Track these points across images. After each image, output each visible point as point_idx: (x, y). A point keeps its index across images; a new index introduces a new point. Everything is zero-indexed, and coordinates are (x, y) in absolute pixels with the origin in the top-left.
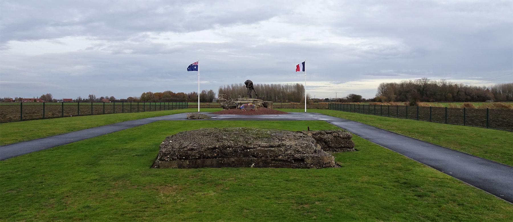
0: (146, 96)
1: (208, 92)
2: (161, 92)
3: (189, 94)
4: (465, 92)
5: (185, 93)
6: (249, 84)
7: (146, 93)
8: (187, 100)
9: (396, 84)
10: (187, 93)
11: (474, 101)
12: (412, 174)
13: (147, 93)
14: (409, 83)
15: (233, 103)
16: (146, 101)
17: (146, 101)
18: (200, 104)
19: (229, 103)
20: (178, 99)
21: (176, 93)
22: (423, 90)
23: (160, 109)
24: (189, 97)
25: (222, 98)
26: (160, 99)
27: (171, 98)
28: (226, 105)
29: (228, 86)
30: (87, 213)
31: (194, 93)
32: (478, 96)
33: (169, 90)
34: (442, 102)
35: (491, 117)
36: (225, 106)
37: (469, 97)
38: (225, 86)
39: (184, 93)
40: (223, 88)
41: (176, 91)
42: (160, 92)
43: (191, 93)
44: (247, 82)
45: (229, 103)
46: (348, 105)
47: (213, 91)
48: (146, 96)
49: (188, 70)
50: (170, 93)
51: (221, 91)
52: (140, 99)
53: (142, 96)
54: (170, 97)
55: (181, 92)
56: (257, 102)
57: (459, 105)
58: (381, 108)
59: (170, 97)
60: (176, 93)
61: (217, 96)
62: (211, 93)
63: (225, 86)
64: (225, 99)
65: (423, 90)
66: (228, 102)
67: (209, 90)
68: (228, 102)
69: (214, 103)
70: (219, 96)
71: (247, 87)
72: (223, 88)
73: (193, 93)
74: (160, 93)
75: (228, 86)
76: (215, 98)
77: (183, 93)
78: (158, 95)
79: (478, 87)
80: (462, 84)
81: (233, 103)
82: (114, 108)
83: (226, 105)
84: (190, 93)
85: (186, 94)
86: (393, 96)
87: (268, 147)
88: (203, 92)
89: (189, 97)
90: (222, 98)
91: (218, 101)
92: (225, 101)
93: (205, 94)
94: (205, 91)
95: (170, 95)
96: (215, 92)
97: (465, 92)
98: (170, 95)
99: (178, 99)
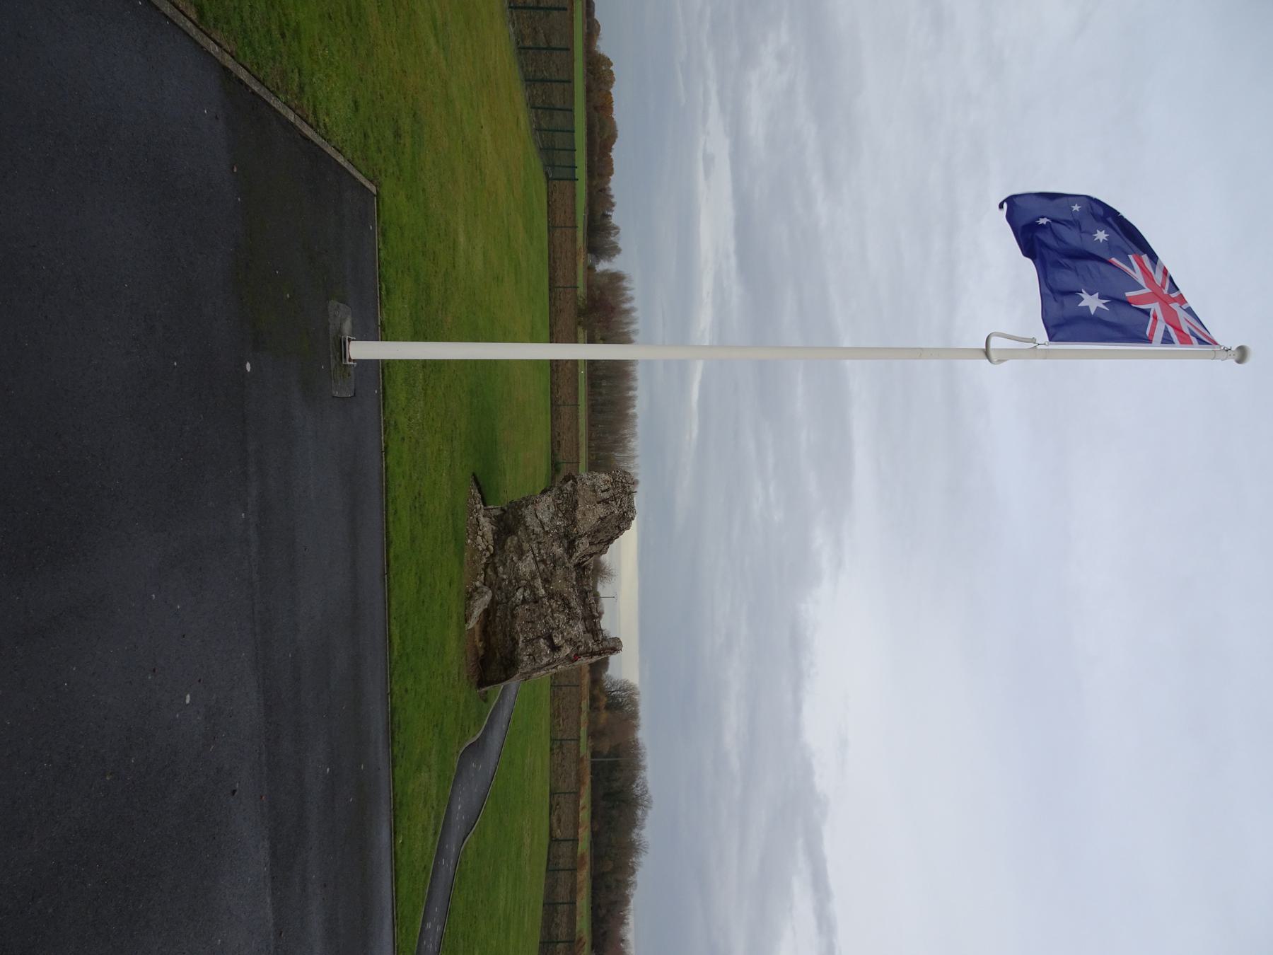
0: (604, 68)
1: (614, 243)
2: (614, 113)
3: (610, 189)
4: (616, 902)
5: (611, 177)
7: (611, 68)
8: (595, 183)
9: (635, 727)
10: (612, 185)
11: (592, 924)
13: (611, 72)
14: (640, 766)
15: (549, 638)
16: (590, 67)
17: (590, 67)
20: (596, 159)
21: (611, 154)
22: (623, 801)
23: (530, 80)
24: (601, 191)
25: (601, 510)
26: (595, 108)
27: (599, 140)
28: (526, 566)
29: (632, 299)
31: (613, 205)
32: (605, 933)
33: (619, 134)
34: (591, 849)
36: (521, 553)
37: (604, 911)
38: (633, 289)
39: (611, 175)
40: (625, 284)
41: (618, 153)
42: (614, 109)
43: (612, 196)
45: (551, 596)
46: (574, 689)
47: (617, 255)
48: (604, 68)
49: (1014, 206)
50: (613, 137)
51: (616, 278)
52: (596, 52)
53: (603, 57)
54: (601, 137)
55: (614, 166)
57: (583, 925)
58: (561, 866)
59: (601, 137)
60: (613, 154)
61: (602, 266)
62: (613, 251)
63: (633, 289)
65: (623, 801)
66: (559, 584)
67: (620, 245)
68: (559, 584)
69: (586, 259)
70: (604, 274)
72: (625, 284)
73: (613, 200)
74: (611, 109)
75: (632, 299)
76: (598, 262)
77: (611, 173)
78: (607, 103)
80: (636, 886)
81: (549, 638)
83: (526, 566)
84: (612, 192)
85: (609, 181)
86: (605, 746)
88: (616, 228)
89: (601, 191)
90: (601, 510)
91: (590, 269)
93: (610, 234)
94: (618, 233)
95: (605, 136)
96: (614, 260)
97: (616, 902)
98: (605, 136)
99: (596, 159)
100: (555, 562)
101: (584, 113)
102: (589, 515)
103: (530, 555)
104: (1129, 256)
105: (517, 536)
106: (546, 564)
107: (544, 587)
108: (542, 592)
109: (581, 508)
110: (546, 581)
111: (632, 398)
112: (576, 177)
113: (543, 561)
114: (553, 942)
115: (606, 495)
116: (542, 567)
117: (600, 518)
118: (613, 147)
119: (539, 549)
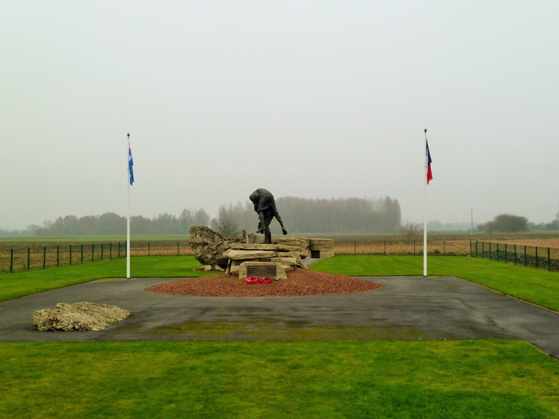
0: (35, 323)
6: (262, 200)
12: (284, 391)
18: (134, 253)
19: (216, 250)
25: (198, 236)
28: (210, 256)
29: (239, 203)
30: (435, 242)
35: (384, 244)
36: (207, 258)
44: (257, 194)
56: (287, 254)
64: (206, 240)
67: (198, 210)
68: (214, 247)
71: (256, 210)
72: (227, 209)
79: (495, 220)
82: (58, 260)
83: (210, 256)
87: (258, 321)
88: (201, 209)
90: (198, 236)
92: (207, 244)
94: (188, 212)
100: (209, 248)
101: (129, 238)
102: (199, 239)
103: (207, 255)
104: (89, 344)
105: (203, 259)
106: (209, 251)
107: (215, 251)
108: (215, 252)
109: (196, 241)
110: (213, 251)
111: (354, 198)
112: (508, 263)
113: (208, 251)
114: (549, 261)
115: (195, 235)
116: (210, 252)
117: (200, 236)
118: (121, 216)
119: (205, 252)
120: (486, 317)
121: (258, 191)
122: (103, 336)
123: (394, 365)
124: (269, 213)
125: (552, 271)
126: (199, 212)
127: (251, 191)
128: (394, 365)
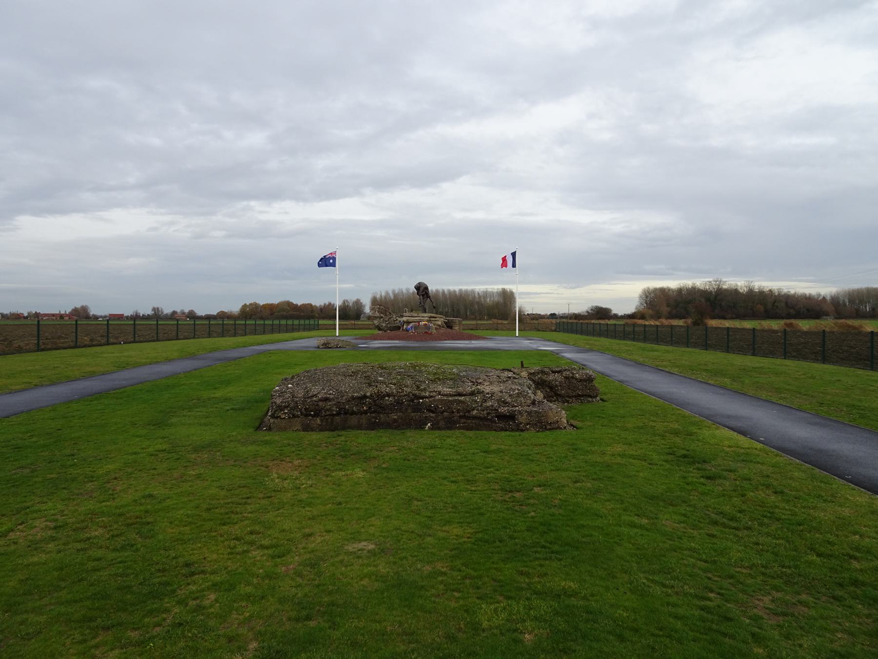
6: (421, 289)
25: (377, 312)
28: (384, 325)
29: (387, 293)
64: (382, 315)
68: (387, 319)
71: (418, 294)
72: (378, 296)
83: (384, 325)
90: (377, 312)
92: (382, 317)
120: (257, 429)
121: (419, 283)
122: (133, 387)
123: (631, 511)
124: (425, 296)
125: (875, 371)
126: (356, 302)
127: (415, 283)
128: (631, 511)
